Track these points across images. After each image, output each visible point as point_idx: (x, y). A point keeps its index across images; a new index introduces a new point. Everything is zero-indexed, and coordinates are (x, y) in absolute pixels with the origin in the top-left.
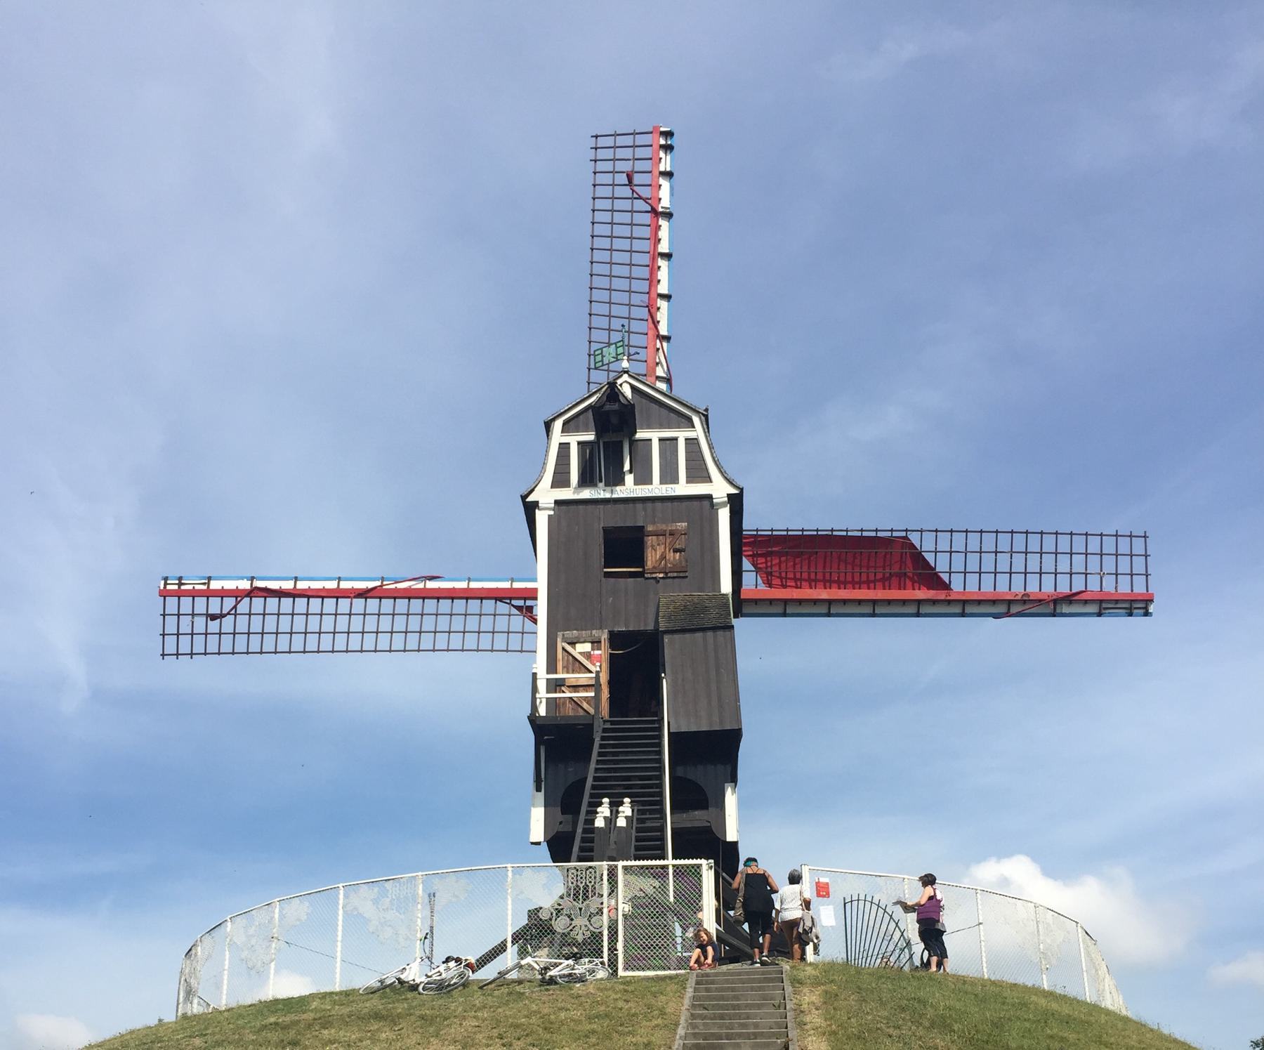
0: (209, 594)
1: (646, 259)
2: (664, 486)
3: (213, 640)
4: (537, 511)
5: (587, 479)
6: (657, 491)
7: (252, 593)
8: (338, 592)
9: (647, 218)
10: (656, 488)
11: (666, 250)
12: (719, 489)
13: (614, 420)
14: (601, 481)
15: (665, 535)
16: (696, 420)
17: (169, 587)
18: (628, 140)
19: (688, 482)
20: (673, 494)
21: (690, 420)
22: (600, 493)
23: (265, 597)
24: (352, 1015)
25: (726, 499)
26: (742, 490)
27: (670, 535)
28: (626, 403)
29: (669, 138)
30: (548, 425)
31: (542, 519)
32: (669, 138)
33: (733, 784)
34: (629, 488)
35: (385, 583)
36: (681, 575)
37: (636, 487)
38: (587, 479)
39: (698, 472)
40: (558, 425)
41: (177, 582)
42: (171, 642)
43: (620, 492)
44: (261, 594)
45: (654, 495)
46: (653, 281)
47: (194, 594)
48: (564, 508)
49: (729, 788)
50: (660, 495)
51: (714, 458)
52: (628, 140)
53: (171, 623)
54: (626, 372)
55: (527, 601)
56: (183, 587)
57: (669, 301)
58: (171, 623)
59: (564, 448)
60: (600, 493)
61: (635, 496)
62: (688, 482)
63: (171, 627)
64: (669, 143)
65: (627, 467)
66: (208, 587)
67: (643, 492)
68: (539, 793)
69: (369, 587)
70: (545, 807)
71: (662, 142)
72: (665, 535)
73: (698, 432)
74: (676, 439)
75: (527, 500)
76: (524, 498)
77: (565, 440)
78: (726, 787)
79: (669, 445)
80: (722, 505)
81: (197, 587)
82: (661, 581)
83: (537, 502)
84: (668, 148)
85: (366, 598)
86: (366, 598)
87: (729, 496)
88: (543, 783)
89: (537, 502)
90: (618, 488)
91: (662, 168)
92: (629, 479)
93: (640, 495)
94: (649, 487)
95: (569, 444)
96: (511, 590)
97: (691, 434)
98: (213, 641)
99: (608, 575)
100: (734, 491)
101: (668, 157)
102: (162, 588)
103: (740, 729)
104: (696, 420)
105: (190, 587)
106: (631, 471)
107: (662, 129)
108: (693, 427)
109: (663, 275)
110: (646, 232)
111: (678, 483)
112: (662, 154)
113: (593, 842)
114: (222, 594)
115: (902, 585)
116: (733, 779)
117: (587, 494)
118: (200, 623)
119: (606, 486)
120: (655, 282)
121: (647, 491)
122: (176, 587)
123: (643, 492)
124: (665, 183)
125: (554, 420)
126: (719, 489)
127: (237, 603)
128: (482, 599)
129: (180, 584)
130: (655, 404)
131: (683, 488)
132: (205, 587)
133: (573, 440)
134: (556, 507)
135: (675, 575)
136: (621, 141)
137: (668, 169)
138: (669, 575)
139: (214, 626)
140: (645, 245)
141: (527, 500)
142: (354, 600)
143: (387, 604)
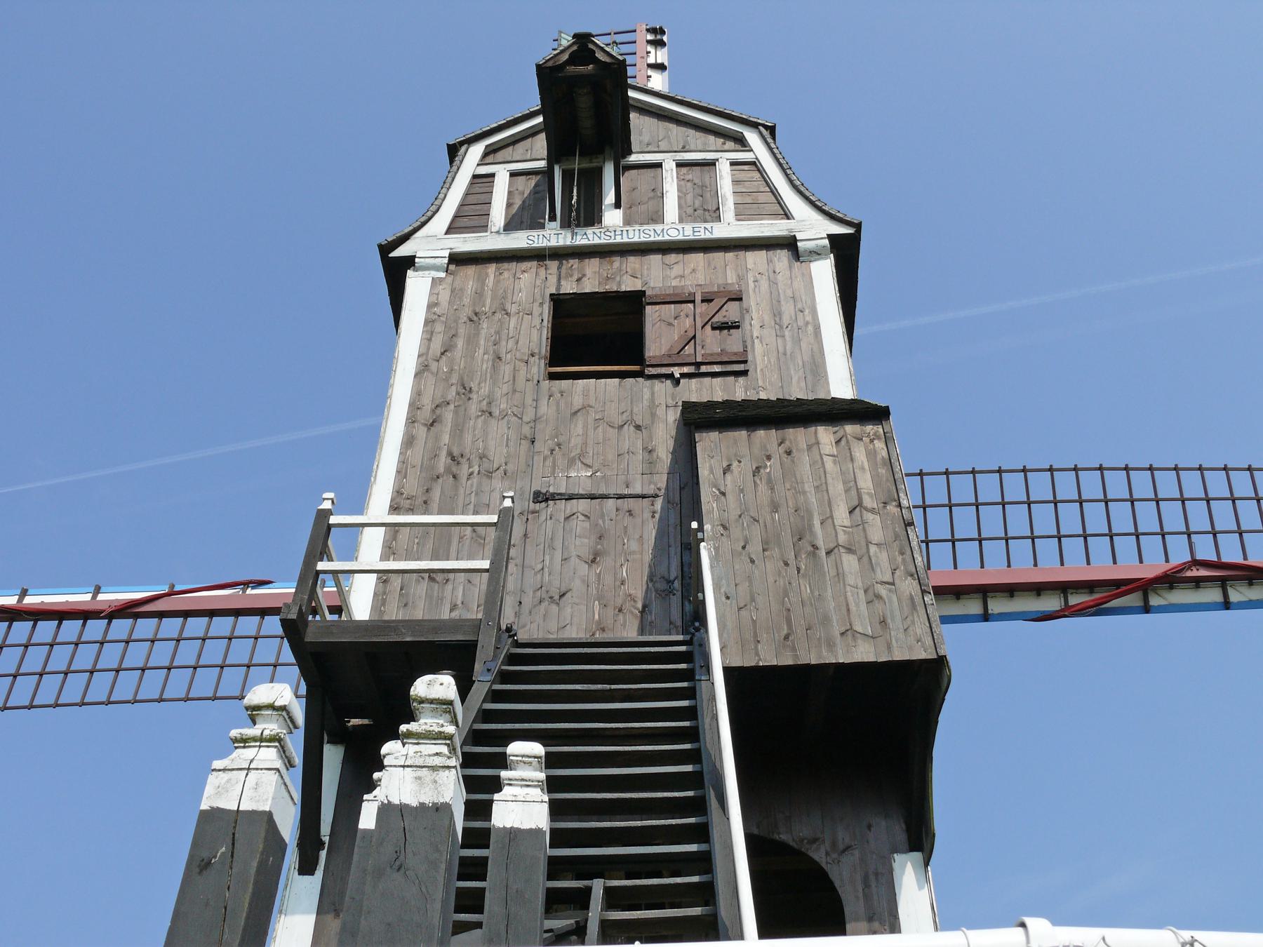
8: (642, 104)
14: (553, 218)
15: (693, 302)
16: (752, 137)
22: (553, 236)
25: (826, 242)
26: (858, 226)
27: (703, 301)
28: (608, 60)
30: (454, 151)
31: (417, 287)
33: (917, 856)
49: (909, 868)
51: (791, 182)
60: (553, 236)
61: (626, 240)
65: (609, 198)
67: (642, 234)
68: (307, 878)
70: (320, 911)
72: (693, 302)
76: (385, 249)
78: (896, 866)
80: (816, 254)
83: (414, 257)
87: (831, 237)
88: (323, 854)
89: (414, 257)
90: (590, 231)
94: (659, 228)
99: (553, 377)
106: (618, 205)
111: (888, 407)
113: (480, 910)
115: (584, 102)
117: (521, 240)
119: (562, 227)
121: (652, 233)
123: (642, 234)
130: (670, 122)
135: (717, 369)
138: (704, 369)
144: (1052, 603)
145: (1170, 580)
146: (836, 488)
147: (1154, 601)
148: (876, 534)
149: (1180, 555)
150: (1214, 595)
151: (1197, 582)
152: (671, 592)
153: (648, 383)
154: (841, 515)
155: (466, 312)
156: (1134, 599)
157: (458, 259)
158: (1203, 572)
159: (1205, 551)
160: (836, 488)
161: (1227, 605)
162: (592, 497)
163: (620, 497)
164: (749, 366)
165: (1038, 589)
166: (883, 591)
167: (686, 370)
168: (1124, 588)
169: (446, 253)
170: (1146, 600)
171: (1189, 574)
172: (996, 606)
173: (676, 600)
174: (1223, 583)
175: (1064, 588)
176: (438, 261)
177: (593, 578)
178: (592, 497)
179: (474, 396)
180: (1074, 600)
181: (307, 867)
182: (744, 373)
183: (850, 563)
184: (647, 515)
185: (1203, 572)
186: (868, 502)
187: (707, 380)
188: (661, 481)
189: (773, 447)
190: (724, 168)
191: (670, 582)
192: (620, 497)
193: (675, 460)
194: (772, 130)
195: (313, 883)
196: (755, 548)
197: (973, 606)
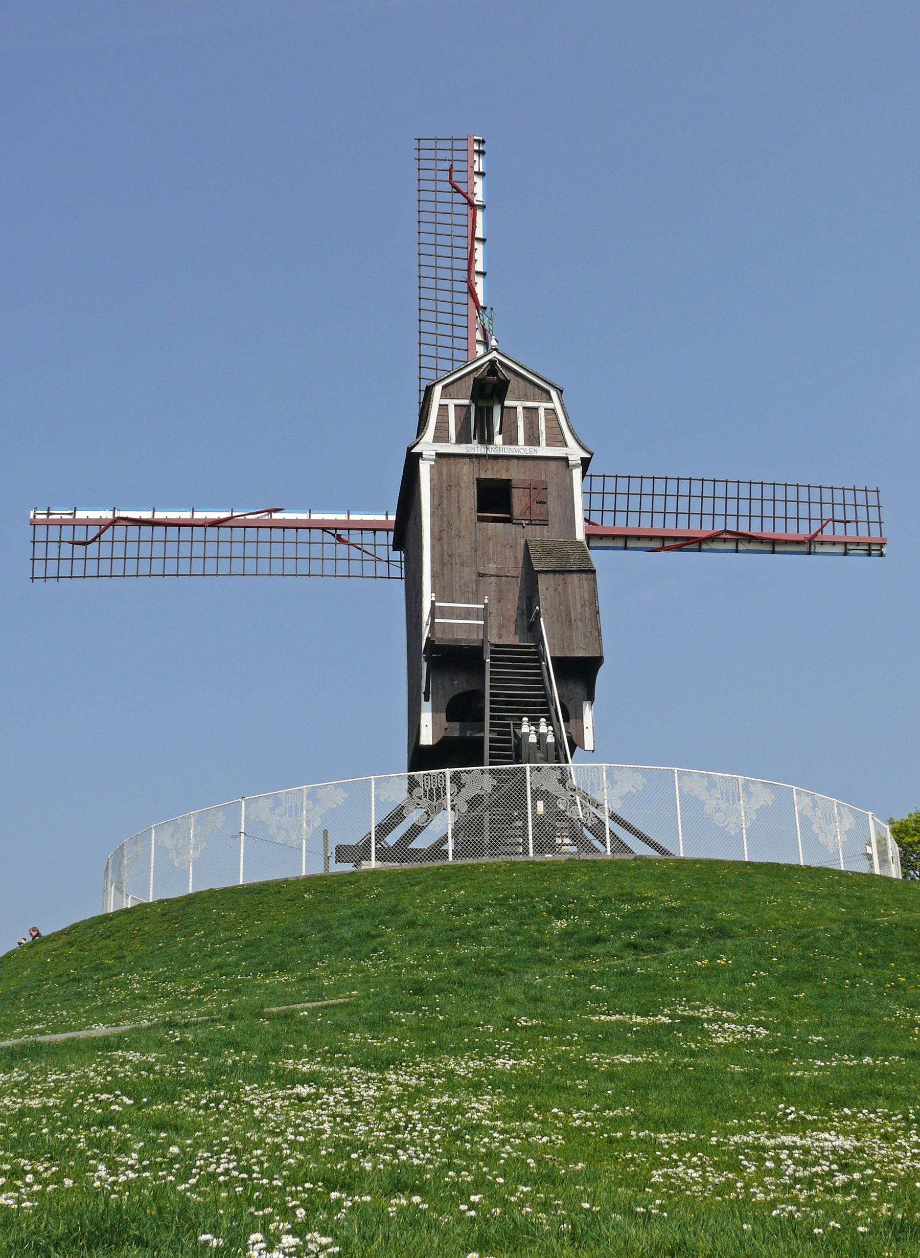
0: (75, 523)
1: (464, 242)
2: (528, 448)
3: (78, 565)
4: (420, 461)
5: (463, 438)
6: (522, 451)
7: (115, 522)
9: (465, 209)
10: (522, 449)
11: (481, 236)
12: (575, 453)
13: (488, 390)
14: (475, 438)
16: (554, 394)
17: (38, 517)
18: (448, 145)
19: (547, 445)
20: (535, 454)
21: (548, 393)
22: (475, 448)
23: (140, 526)
24: (519, 934)
25: (580, 462)
26: (592, 455)
29: (481, 145)
32: (481, 145)
33: (590, 702)
34: (499, 446)
35: (235, 514)
36: (543, 522)
37: (504, 447)
38: (463, 438)
39: (557, 439)
40: (438, 390)
41: (46, 512)
42: (40, 565)
43: (492, 451)
44: (123, 522)
45: (520, 454)
46: (471, 260)
47: (61, 524)
48: (444, 461)
50: (525, 454)
51: (569, 427)
52: (448, 145)
53: (41, 548)
54: (496, 350)
55: (273, 514)
56: (51, 517)
57: (484, 277)
58: (41, 548)
59: (443, 408)
60: (475, 448)
61: (504, 453)
62: (547, 445)
63: (40, 553)
64: (481, 149)
66: (74, 517)
69: (221, 517)
71: (476, 147)
73: (556, 404)
74: (537, 409)
75: (413, 451)
77: (444, 402)
79: (531, 412)
80: (576, 466)
81: (64, 517)
82: (526, 526)
84: (481, 153)
85: (219, 527)
86: (219, 527)
87: (582, 459)
91: (476, 169)
92: (498, 439)
93: (508, 454)
94: (516, 447)
95: (447, 405)
96: (348, 521)
97: (549, 405)
98: (79, 566)
99: (481, 519)
100: (587, 456)
101: (481, 160)
102: (32, 517)
103: (602, 657)
104: (554, 394)
105: (58, 517)
107: (475, 138)
108: (551, 399)
109: (479, 255)
110: (463, 220)
112: (476, 157)
114: (87, 523)
116: (590, 697)
117: (463, 449)
118: (66, 549)
120: (474, 261)
122: (45, 517)
124: (478, 180)
125: (434, 385)
126: (575, 453)
127: (102, 532)
128: (310, 528)
129: (49, 514)
131: (543, 450)
132: (71, 517)
133: (451, 403)
134: (437, 459)
135: (538, 522)
136: (441, 144)
137: (481, 170)
138: (533, 522)
139: (79, 550)
140: (464, 231)
141: (413, 451)
142: (208, 528)
143: (238, 533)
144: (656, 544)
145: (713, 538)
146: (578, 597)
147: (704, 547)
148: (588, 616)
149: (719, 527)
150: (732, 546)
151: (725, 540)
152: (523, 614)
153: (514, 526)
154: (579, 606)
155: (445, 485)
156: (696, 546)
157: (439, 455)
158: (728, 536)
159: (732, 527)
160: (578, 597)
161: (737, 551)
162: (497, 576)
163: (507, 576)
164: (549, 522)
165: (651, 538)
166: (588, 635)
167: (527, 522)
168: (691, 541)
169: (434, 453)
170: (700, 546)
171: (722, 536)
172: (630, 544)
173: (525, 617)
174: (737, 541)
175: (663, 538)
176: (431, 457)
177: (499, 608)
178: (497, 576)
179: (453, 528)
180: (667, 544)
181: (427, 700)
182: (547, 525)
183: (580, 623)
184: (515, 584)
185: (728, 536)
186: (587, 604)
187: (534, 526)
188: (520, 571)
189: (561, 582)
190: (542, 413)
191: (523, 611)
192: (507, 576)
193: (524, 563)
194: (562, 391)
195: (430, 703)
196: (555, 618)
197: (621, 544)
